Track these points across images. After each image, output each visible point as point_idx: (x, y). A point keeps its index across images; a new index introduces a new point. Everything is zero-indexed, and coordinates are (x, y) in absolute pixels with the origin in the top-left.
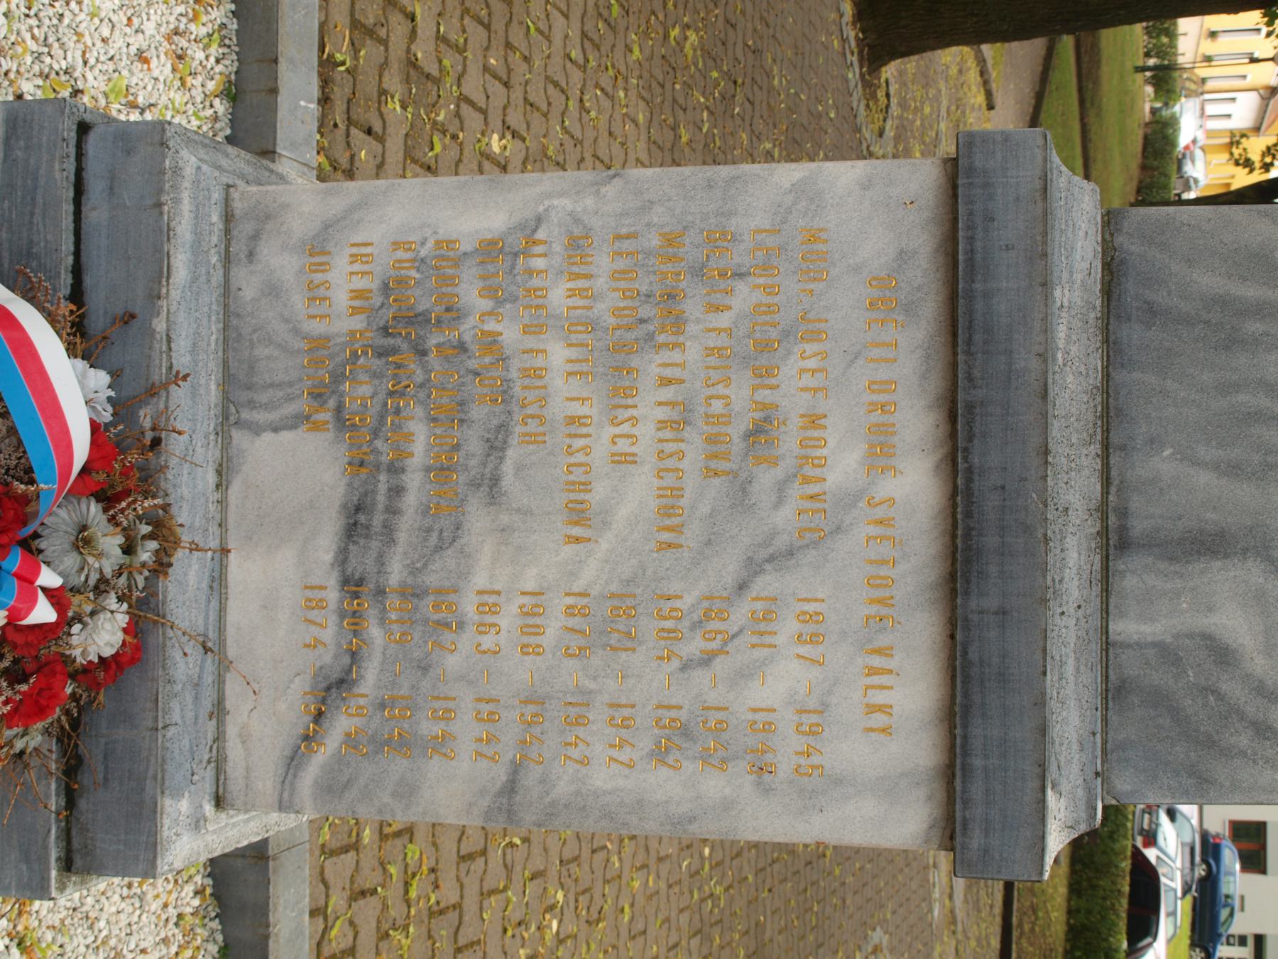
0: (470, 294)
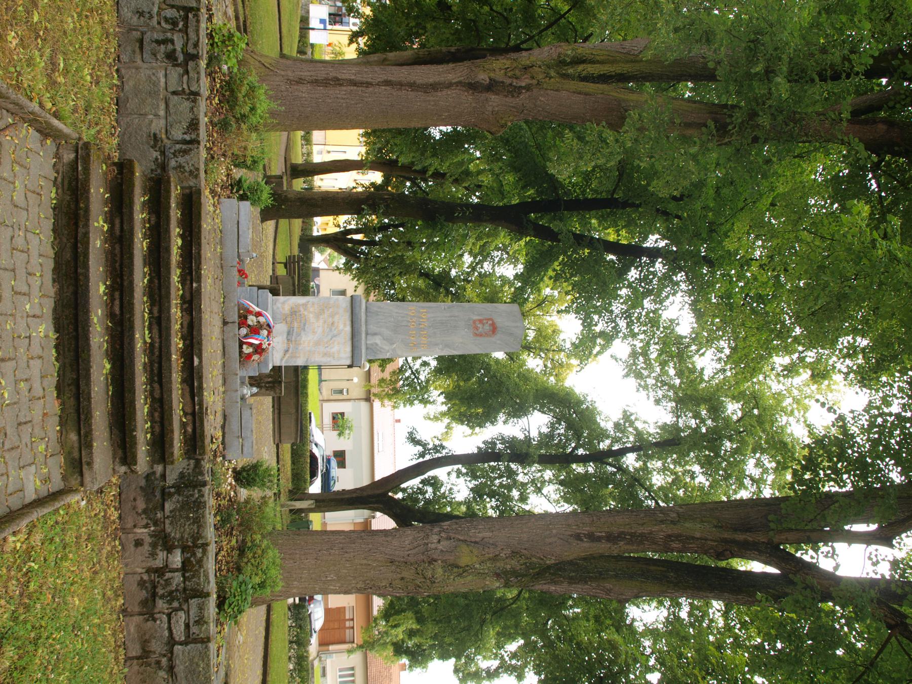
0: (301, 309)
